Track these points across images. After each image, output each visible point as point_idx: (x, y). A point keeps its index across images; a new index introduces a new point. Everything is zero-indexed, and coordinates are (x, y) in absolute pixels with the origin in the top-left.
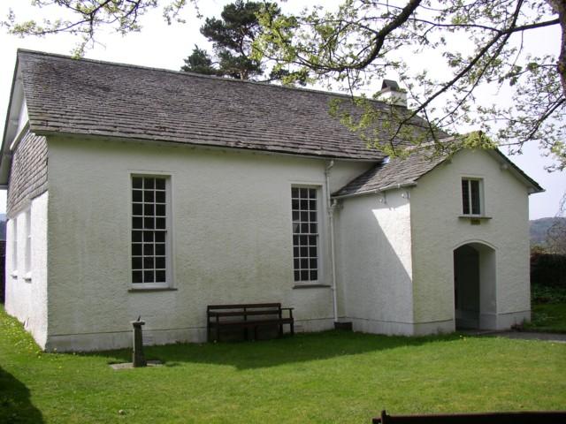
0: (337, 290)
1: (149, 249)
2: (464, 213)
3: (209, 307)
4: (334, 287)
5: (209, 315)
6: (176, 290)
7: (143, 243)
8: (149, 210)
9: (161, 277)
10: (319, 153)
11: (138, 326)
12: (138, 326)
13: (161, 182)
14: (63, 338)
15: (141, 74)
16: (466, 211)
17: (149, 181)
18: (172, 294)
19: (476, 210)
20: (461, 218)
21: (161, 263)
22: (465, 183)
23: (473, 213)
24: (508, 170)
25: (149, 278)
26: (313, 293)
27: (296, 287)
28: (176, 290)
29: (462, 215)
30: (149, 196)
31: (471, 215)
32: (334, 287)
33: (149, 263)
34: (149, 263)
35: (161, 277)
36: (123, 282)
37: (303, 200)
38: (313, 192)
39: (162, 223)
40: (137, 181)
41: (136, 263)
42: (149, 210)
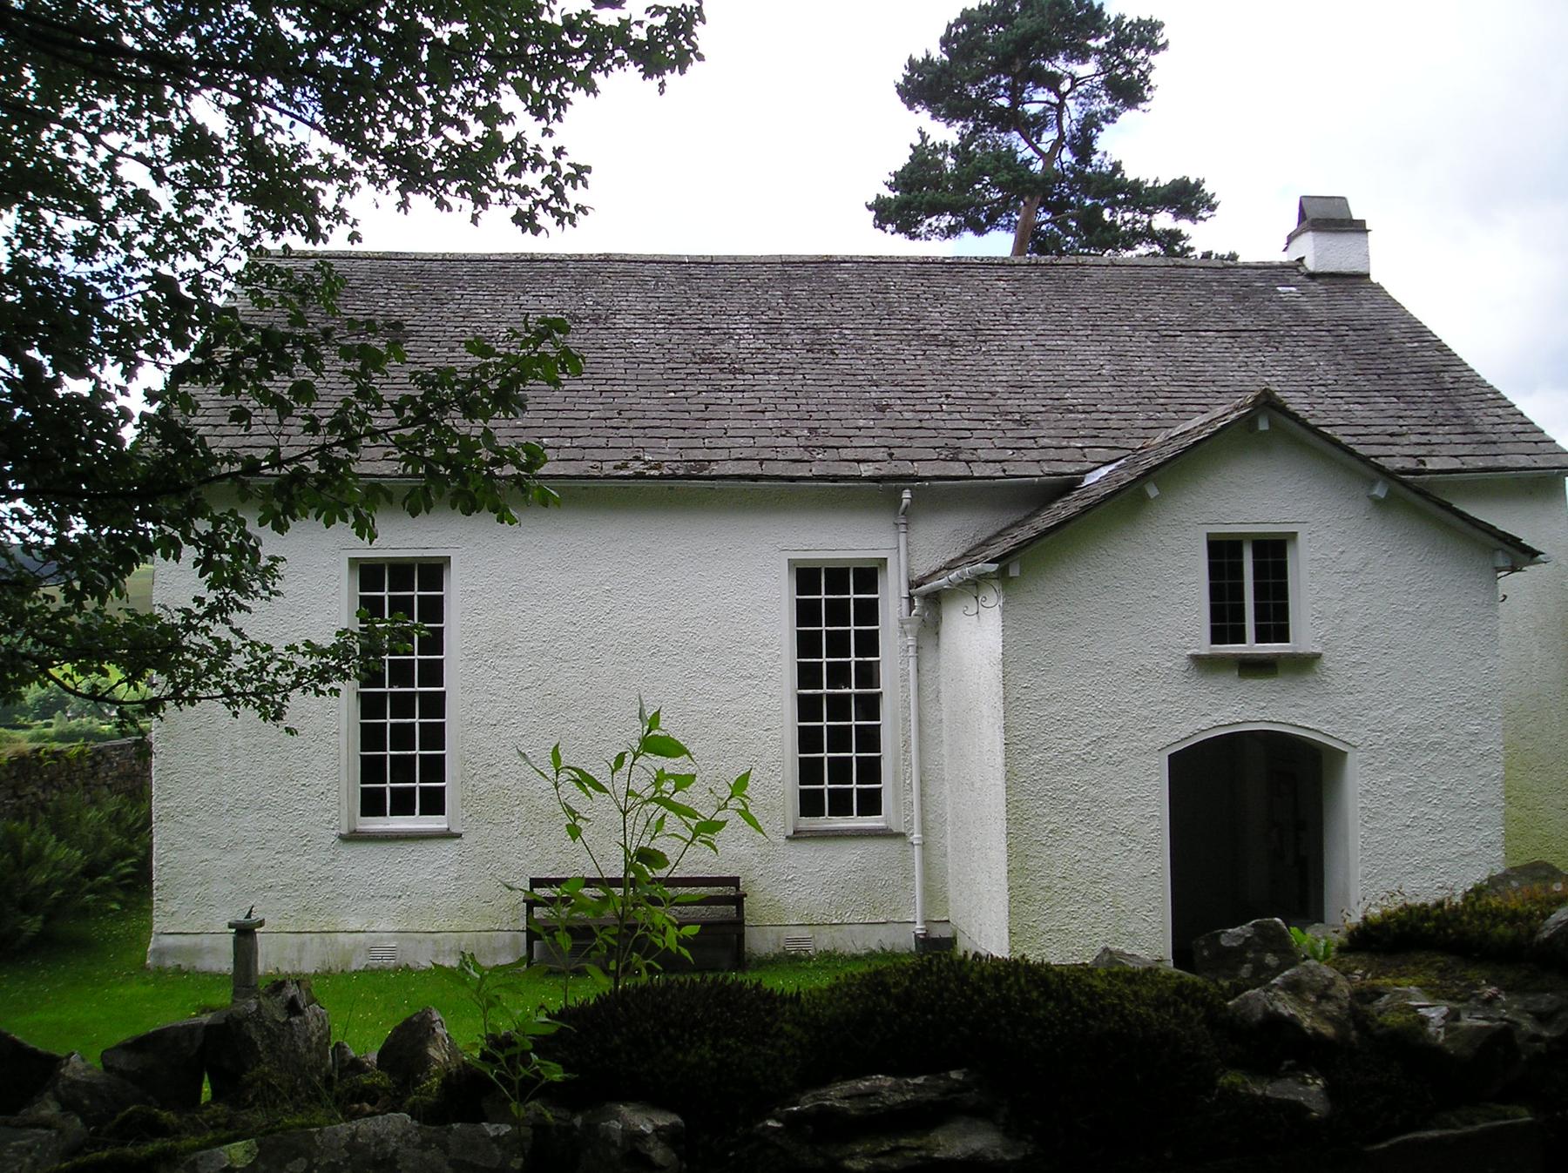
0: (924, 845)
1: (403, 737)
2: (1217, 636)
3: (536, 883)
4: (916, 837)
5: (531, 904)
6: (459, 836)
7: (389, 721)
8: (838, 644)
9: (433, 802)
10: (866, 470)
11: (245, 933)
12: (245, 933)
13: (433, 572)
14: (185, 940)
15: (540, 274)
16: (1225, 625)
17: (837, 576)
18: (449, 847)
19: (1275, 624)
20: (1204, 664)
21: (435, 769)
22: (1223, 552)
23: (1261, 637)
24: (1391, 496)
25: (403, 805)
26: (850, 855)
27: (797, 836)
28: (459, 836)
29: (1205, 647)
30: (838, 612)
31: (1251, 647)
32: (916, 837)
33: (403, 769)
34: (403, 769)
35: (433, 802)
36: (328, 816)
37: (833, 609)
38: (868, 576)
39: (433, 673)
40: (806, 577)
41: (371, 769)
42: (838, 644)
